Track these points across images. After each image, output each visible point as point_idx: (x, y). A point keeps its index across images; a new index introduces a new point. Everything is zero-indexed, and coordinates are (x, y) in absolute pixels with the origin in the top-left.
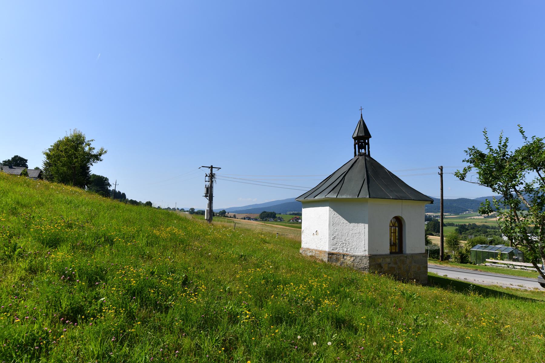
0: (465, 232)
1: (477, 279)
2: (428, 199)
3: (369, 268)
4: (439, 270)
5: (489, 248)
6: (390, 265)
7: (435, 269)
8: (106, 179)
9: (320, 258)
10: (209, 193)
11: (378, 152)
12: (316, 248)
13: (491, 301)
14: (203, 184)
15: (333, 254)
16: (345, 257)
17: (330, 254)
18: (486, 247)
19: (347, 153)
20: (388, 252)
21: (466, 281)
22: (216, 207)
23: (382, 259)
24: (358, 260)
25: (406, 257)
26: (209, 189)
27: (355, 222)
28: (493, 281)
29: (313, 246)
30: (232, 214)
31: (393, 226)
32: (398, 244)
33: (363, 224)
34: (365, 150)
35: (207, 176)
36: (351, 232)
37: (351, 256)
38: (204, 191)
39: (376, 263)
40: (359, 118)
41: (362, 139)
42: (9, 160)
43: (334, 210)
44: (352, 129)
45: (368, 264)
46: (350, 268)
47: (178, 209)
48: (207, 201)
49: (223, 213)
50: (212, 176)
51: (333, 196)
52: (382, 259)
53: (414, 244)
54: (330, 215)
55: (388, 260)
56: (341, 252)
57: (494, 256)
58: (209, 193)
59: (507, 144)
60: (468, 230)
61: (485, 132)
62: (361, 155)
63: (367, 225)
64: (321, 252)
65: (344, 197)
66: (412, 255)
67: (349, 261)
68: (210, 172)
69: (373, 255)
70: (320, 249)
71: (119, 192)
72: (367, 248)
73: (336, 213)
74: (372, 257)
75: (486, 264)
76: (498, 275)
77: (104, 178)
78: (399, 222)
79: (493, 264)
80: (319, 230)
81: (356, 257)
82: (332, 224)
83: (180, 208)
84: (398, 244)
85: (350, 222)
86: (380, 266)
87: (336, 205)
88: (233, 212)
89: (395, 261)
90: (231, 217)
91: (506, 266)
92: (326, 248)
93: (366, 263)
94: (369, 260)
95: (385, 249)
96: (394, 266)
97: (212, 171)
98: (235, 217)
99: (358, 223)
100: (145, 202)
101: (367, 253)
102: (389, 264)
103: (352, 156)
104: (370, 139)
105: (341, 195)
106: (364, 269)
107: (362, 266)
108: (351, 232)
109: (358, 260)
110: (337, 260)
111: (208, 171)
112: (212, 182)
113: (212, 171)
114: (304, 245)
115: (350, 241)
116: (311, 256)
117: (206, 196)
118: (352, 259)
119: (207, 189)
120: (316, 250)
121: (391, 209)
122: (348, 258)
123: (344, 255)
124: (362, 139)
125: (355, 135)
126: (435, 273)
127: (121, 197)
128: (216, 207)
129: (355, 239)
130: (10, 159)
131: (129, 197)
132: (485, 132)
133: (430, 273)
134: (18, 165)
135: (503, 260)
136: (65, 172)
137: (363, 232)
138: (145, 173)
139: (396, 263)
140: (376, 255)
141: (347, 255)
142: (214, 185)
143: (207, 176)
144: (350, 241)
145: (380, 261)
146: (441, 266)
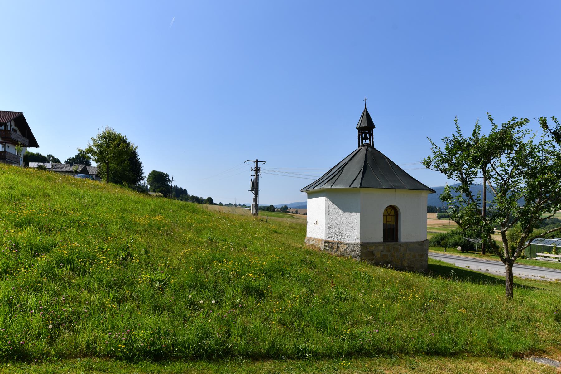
0: (544, 227)
1: (498, 271)
2: (425, 188)
3: (361, 255)
4: (457, 261)
5: (544, 242)
6: (383, 253)
7: (437, 256)
8: (167, 175)
9: (318, 246)
10: (255, 187)
11: (382, 143)
12: (316, 237)
13: (458, 285)
14: (249, 178)
15: (328, 242)
16: (339, 245)
17: (326, 242)
18: (541, 241)
19: (351, 143)
20: (381, 239)
21: (468, 269)
22: (262, 202)
23: (374, 247)
24: (350, 248)
25: (400, 245)
26: (255, 184)
27: (349, 212)
28: (521, 273)
29: (314, 236)
30: (294, 210)
31: (389, 215)
32: (391, 232)
33: (355, 213)
34: (370, 141)
35: (252, 170)
36: (345, 221)
37: (345, 244)
38: (250, 185)
39: (367, 251)
40: (364, 109)
41: (366, 128)
42: (73, 158)
43: (330, 200)
44: (355, 120)
45: (359, 252)
46: (308, 252)
47: (240, 205)
48: (252, 195)
49: (271, 209)
50: (257, 170)
51: (328, 186)
52: (374, 247)
53: (407, 233)
54: (326, 204)
55: (381, 248)
56: (336, 240)
57: (549, 250)
58: (255, 187)
59: (480, 132)
60: (548, 225)
61: (456, 121)
62: (363, 146)
63: (359, 214)
64: (319, 240)
65: (338, 187)
66: (407, 244)
67: (342, 248)
68: (255, 166)
69: (365, 243)
70: (319, 238)
71: (181, 188)
72: (359, 236)
73: (332, 203)
74: (363, 245)
75: (537, 258)
76: (540, 268)
77: (164, 174)
78: (393, 213)
79: (544, 258)
80: (321, 221)
81: (349, 245)
82: (328, 213)
83: (242, 204)
84: (391, 232)
85: (344, 212)
86: (372, 253)
87: (332, 195)
88: (295, 208)
89: (389, 248)
90: (292, 213)
91: (557, 260)
92: (323, 237)
93: (358, 250)
94: (361, 247)
95: (379, 237)
96: (387, 253)
97: (257, 165)
98: (297, 212)
99: (351, 212)
100: (206, 199)
101: (359, 241)
102: (382, 251)
103: (356, 147)
104: (374, 130)
105: (336, 185)
106: (356, 256)
107: (354, 253)
108: (345, 221)
109: (350, 248)
110: (332, 248)
111: (253, 165)
112: (257, 176)
113: (257, 165)
114: (308, 235)
115: (344, 229)
116: (312, 245)
117: (252, 191)
118: (346, 247)
119: (253, 183)
120: (316, 239)
121: (383, 199)
122: (342, 246)
123: (338, 243)
124: (366, 128)
125: (358, 127)
126: (453, 263)
127: (181, 194)
128: (261, 203)
129: (348, 227)
130: (74, 157)
131: (190, 193)
132: (456, 121)
133: (432, 260)
134: (81, 163)
135: (557, 254)
136: (115, 169)
137: (356, 220)
138: (205, 170)
139: (389, 251)
140: (368, 243)
141: (341, 243)
142: (260, 179)
143: (252, 170)
144: (344, 229)
145: (372, 249)
146: (480, 259)
